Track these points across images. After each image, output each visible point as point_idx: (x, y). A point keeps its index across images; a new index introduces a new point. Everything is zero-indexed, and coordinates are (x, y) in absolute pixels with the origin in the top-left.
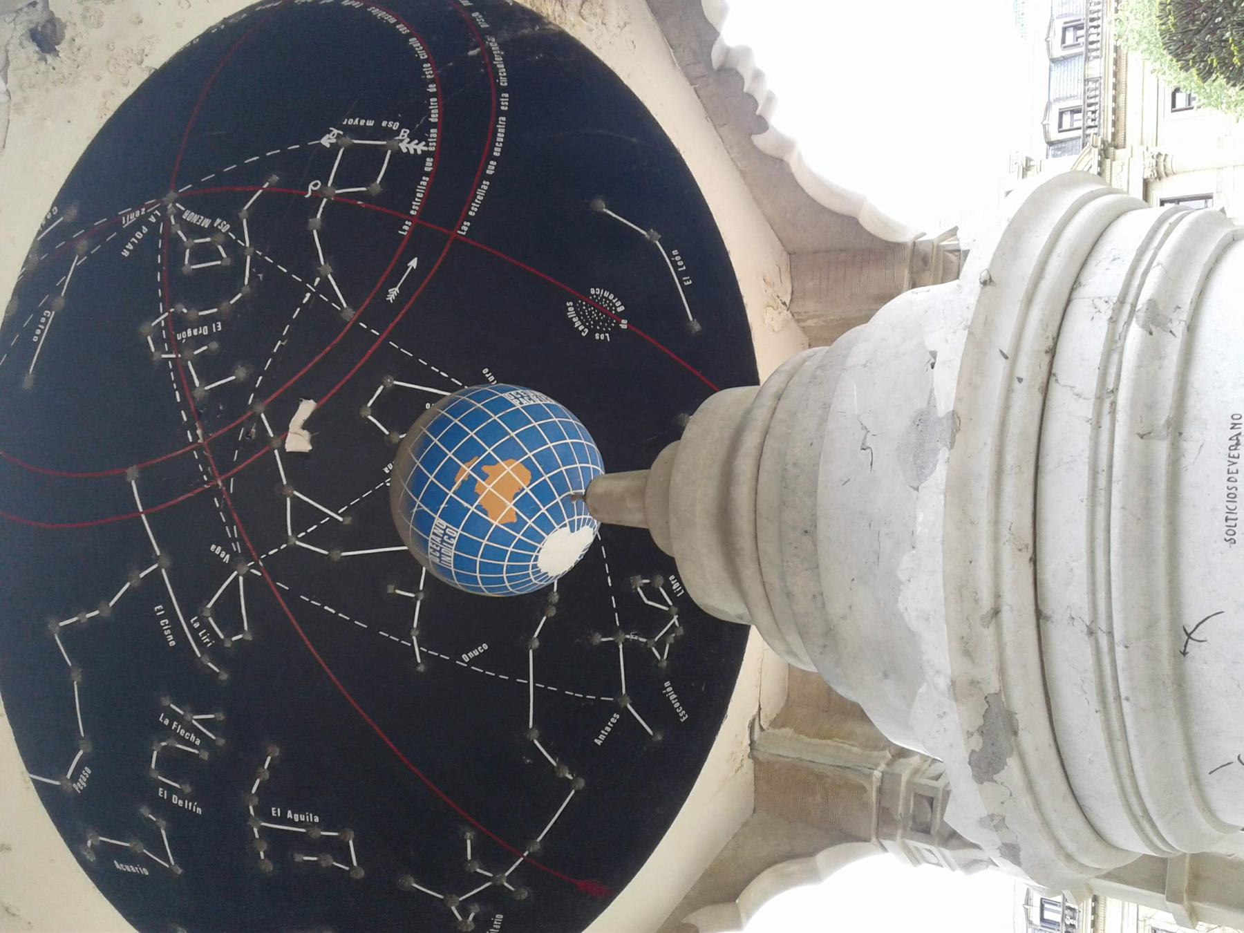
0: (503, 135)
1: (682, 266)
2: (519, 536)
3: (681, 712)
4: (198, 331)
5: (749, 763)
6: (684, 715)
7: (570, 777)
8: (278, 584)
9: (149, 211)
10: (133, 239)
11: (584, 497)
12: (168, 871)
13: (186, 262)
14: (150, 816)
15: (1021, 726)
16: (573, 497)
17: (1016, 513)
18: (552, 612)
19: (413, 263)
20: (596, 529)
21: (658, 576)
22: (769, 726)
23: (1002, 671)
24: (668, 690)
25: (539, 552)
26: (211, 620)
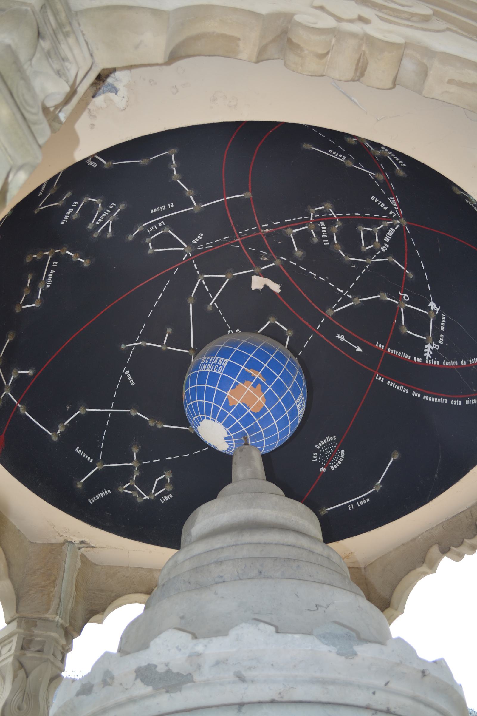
0: (436, 401)
1: (360, 504)
2: (221, 408)
3: (93, 500)
4: (325, 233)
5: (61, 540)
6: (92, 501)
7: (58, 432)
8: (178, 268)
9: (396, 211)
10: (380, 202)
11: (247, 444)
12: (37, 206)
13: (365, 228)
14: (65, 197)
15: (173, 695)
16: (246, 439)
17: (300, 694)
18: (151, 424)
19: (359, 349)
20: (227, 452)
21: (172, 488)
22: (82, 553)
23: (207, 683)
24: (106, 492)
25: (212, 420)
26: (162, 232)
